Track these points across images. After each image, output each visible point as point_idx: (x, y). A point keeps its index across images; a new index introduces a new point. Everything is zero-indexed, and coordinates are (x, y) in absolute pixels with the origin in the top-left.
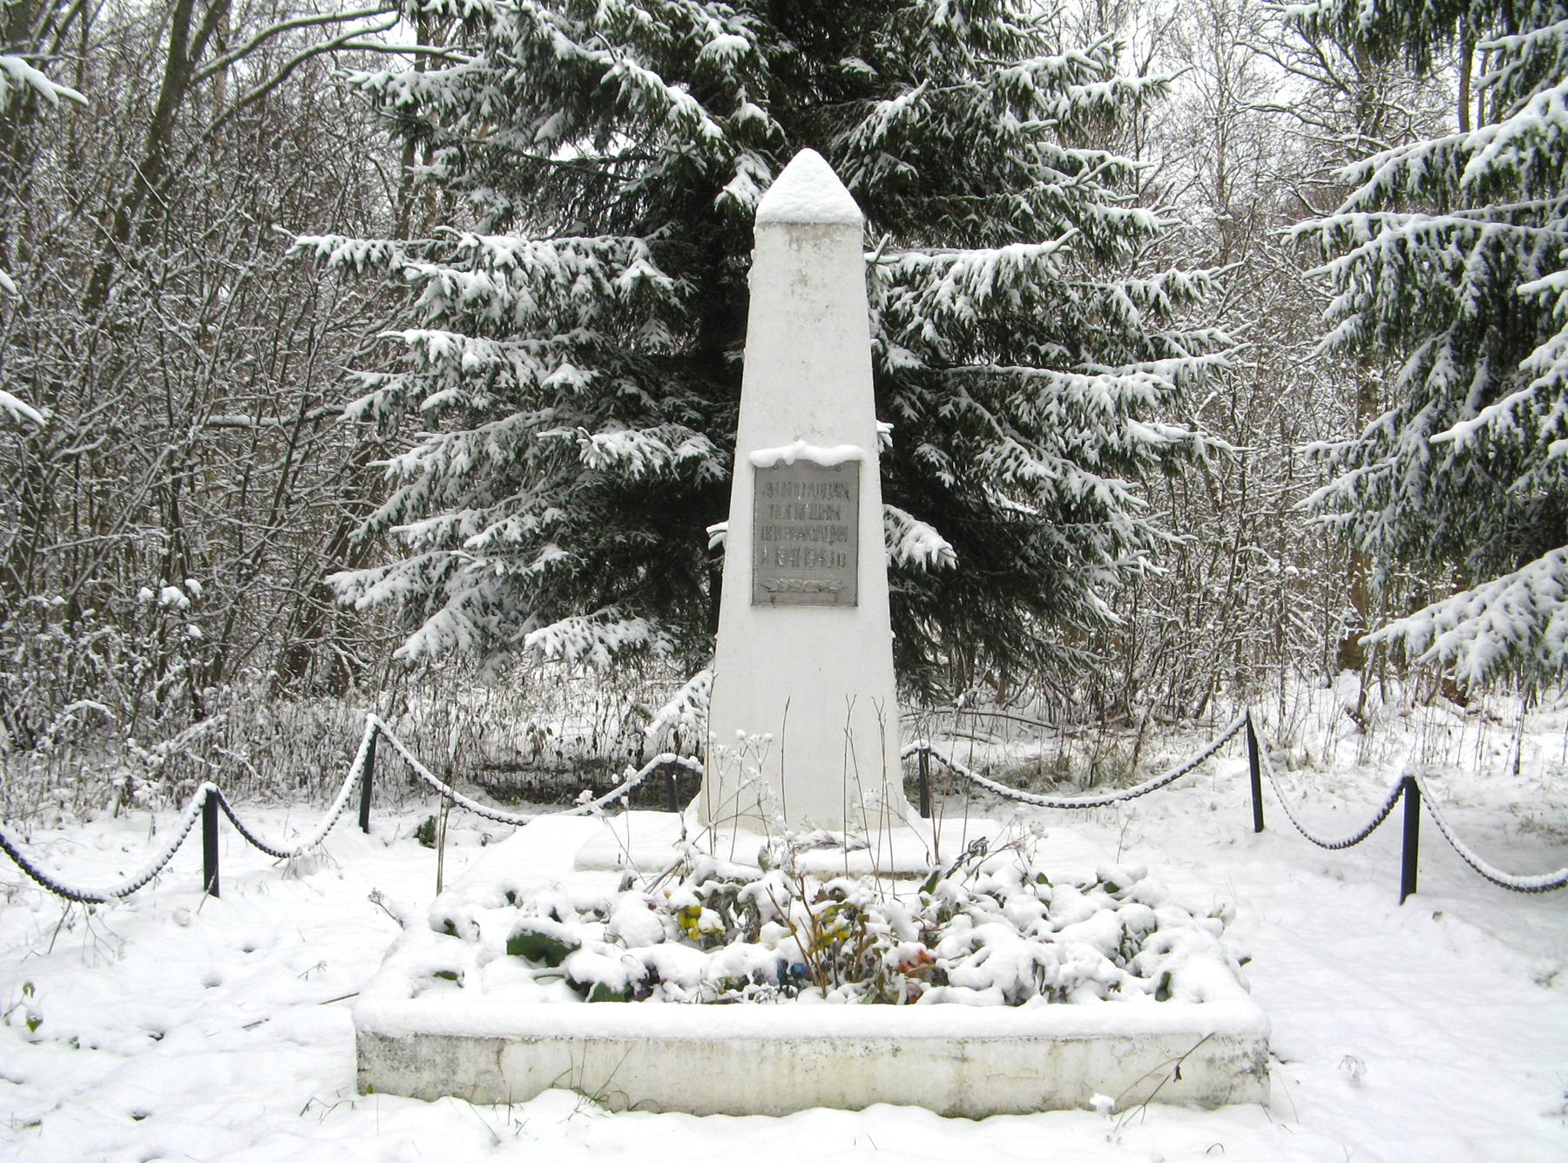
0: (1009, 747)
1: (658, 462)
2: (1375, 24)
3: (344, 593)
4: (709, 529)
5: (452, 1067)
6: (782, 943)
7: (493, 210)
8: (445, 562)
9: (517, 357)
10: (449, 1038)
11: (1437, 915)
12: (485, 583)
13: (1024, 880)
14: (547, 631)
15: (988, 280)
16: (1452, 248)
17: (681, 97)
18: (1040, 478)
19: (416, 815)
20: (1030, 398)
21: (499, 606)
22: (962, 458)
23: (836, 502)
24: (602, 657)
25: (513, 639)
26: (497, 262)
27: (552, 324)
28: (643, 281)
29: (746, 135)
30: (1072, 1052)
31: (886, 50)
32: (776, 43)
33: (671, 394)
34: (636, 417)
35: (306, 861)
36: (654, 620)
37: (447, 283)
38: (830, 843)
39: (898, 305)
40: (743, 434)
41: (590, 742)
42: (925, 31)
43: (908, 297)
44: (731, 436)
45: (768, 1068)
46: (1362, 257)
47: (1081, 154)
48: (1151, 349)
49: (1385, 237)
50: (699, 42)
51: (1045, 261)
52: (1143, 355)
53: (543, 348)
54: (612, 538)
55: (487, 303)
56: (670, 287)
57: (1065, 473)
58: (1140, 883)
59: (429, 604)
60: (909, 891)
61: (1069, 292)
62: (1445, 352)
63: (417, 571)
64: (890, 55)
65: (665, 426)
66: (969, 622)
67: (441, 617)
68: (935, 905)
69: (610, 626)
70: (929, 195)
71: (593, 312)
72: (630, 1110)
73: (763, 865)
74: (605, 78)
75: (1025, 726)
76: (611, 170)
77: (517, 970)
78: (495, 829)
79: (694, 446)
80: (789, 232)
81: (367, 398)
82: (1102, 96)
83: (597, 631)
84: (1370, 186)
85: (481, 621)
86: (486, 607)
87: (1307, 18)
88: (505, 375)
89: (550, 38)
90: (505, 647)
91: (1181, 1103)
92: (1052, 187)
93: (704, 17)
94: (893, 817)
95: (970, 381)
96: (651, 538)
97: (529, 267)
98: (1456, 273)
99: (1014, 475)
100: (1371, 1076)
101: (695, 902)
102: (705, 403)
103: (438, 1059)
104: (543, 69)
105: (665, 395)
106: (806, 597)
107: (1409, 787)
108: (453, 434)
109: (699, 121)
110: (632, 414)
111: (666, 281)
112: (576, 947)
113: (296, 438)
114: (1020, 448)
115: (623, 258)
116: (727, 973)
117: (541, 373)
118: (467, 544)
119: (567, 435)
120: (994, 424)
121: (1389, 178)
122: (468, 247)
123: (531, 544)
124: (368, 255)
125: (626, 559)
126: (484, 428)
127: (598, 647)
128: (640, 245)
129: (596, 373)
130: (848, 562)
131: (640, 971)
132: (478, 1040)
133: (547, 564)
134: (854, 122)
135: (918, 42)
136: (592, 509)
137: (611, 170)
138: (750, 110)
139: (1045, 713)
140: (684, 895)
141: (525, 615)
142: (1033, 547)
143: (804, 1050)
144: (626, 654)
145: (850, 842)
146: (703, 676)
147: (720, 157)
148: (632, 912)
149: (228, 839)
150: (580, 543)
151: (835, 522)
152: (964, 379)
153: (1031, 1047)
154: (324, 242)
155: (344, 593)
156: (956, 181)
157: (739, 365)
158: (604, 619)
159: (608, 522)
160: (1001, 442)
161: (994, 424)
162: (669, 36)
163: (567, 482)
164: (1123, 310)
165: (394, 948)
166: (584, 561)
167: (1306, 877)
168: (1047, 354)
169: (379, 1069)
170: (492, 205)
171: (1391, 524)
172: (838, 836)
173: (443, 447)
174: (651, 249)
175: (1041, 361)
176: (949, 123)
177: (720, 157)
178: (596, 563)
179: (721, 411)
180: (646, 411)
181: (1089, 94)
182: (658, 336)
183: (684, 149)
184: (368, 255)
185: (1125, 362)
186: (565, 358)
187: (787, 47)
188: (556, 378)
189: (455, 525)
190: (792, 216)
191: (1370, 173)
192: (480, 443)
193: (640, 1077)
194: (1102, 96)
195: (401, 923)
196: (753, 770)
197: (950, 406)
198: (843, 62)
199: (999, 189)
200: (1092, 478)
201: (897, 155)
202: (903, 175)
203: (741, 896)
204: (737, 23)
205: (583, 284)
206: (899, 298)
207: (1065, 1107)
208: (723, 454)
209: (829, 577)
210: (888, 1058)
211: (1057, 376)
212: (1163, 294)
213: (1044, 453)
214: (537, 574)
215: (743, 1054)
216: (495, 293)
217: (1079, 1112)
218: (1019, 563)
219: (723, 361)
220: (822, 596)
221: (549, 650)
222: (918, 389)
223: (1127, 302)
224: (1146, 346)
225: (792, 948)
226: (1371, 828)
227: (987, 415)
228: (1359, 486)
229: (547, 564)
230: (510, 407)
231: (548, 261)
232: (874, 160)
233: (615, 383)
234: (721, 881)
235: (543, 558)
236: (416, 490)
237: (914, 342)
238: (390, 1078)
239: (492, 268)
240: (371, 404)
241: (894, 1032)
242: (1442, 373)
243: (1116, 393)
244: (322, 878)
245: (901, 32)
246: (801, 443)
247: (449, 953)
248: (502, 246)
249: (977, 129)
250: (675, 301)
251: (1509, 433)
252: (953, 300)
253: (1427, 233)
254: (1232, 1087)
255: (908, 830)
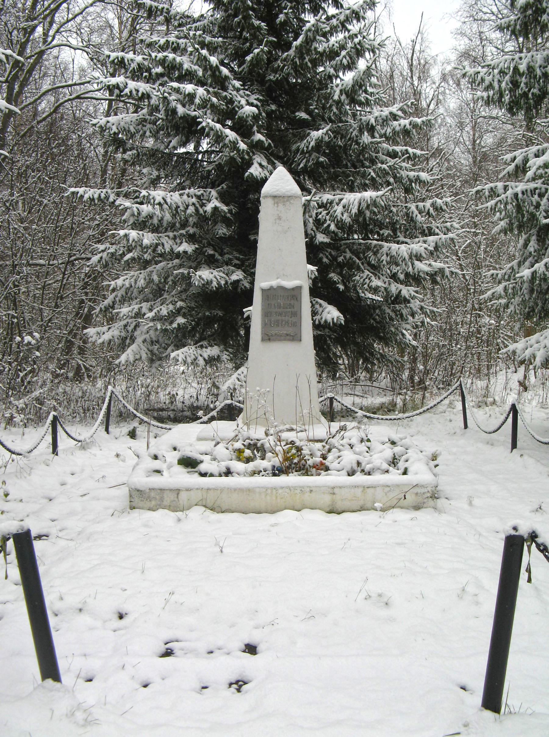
0: (373, 399)
1: (223, 282)
2: (513, 101)
3: (92, 337)
4: (244, 310)
5: (162, 499)
6: (273, 459)
7: (152, 176)
8: (134, 324)
9: (164, 240)
10: (161, 490)
11: (522, 455)
12: (152, 332)
13: (362, 441)
14: (179, 352)
15: (356, 207)
16: (536, 196)
17: (231, 135)
18: (379, 287)
19: (126, 428)
20: (375, 253)
21: (157, 342)
22: (346, 279)
23: (292, 302)
24: (201, 362)
25: (164, 355)
26: (156, 202)
27: (178, 225)
28: (216, 209)
29: (256, 147)
30: (370, 491)
31: (315, 109)
32: (269, 105)
33: (228, 253)
34: (213, 263)
35: (87, 443)
36: (222, 347)
37: (135, 210)
38: (292, 430)
39: (320, 217)
40: (259, 270)
41: (195, 397)
42: (331, 101)
43: (324, 213)
44: (252, 270)
45: (268, 497)
46: (500, 201)
47: (398, 149)
48: (427, 231)
49: (510, 192)
50: (237, 109)
51: (378, 200)
52: (423, 234)
53: (175, 236)
54: (204, 313)
55: (151, 217)
56: (227, 211)
57: (390, 284)
58: (403, 441)
59: (128, 341)
60: (319, 445)
61: (392, 208)
62: (534, 238)
63: (123, 328)
64: (316, 111)
65: (225, 267)
66: (352, 346)
67: (134, 347)
68: (327, 447)
69: (204, 349)
70: (334, 168)
71: (195, 220)
72: (222, 512)
73: (267, 434)
74: (199, 127)
75: (381, 391)
76: (200, 157)
77: (181, 469)
78: (158, 431)
79: (237, 275)
80: (274, 200)
81: (99, 256)
82: (405, 126)
83: (199, 351)
84: (513, 165)
85: (150, 348)
86: (152, 342)
87: (485, 98)
88: (160, 248)
89: (176, 108)
90: (160, 359)
91: (407, 508)
92: (384, 166)
93: (239, 98)
94: (315, 420)
95: (350, 247)
96: (220, 313)
97: (169, 204)
98: (538, 206)
99: (368, 285)
100: (476, 502)
101: (243, 447)
102: (241, 257)
103: (157, 497)
104: (173, 119)
105: (225, 254)
106: (282, 338)
107: (514, 410)
108: (139, 272)
109: (238, 143)
110: (212, 262)
111: (225, 208)
112: (202, 462)
113: (65, 270)
114: (371, 274)
115: (207, 198)
116: (254, 469)
117: (175, 247)
118: (145, 317)
119: (186, 272)
120: (360, 264)
121: (521, 162)
122: (144, 196)
123: (172, 316)
124: (100, 196)
125: (209, 321)
126: (149, 269)
127: (200, 358)
128: (214, 193)
129: (197, 246)
130: (298, 325)
131: (224, 470)
132: (171, 490)
133: (178, 324)
134: (302, 138)
135: (328, 106)
136: (196, 302)
137: (200, 157)
138: (258, 137)
139: (389, 385)
140: (238, 445)
141: (169, 345)
142: (377, 315)
143: (280, 491)
144: (211, 361)
145: (299, 429)
146: (243, 369)
147: (246, 157)
148: (221, 451)
149: (61, 433)
150: (191, 316)
151: (293, 310)
152: (348, 246)
153: (356, 489)
154: (81, 190)
155: (92, 337)
156: (345, 163)
157: (256, 242)
158: (202, 347)
159: (202, 307)
160: (363, 272)
161: (360, 264)
162: (225, 107)
163: (185, 290)
164: (414, 216)
165: (137, 464)
166: (193, 323)
167: (480, 445)
168: (383, 234)
169: (137, 501)
170: (151, 174)
171: (518, 305)
172: (294, 427)
173: (135, 277)
174: (218, 193)
175: (382, 238)
176: (341, 139)
177: (246, 157)
178: (198, 324)
179: (248, 260)
180: (217, 261)
181: (400, 125)
182: (222, 230)
183: (232, 154)
184: (100, 196)
185: (416, 237)
186: (184, 240)
187: (273, 107)
188: (181, 249)
189: (140, 309)
190: (275, 194)
191: (515, 158)
192: (150, 275)
193: (226, 500)
194: (405, 126)
195: (138, 456)
196: (263, 402)
197: (342, 257)
198: (297, 114)
199: (363, 166)
200: (401, 287)
201: (318, 153)
202: (322, 162)
203: (259, 445)
204: (252, 99)
205: (191, 210)
206: (321, 213)
207: (368, 510)
208: (249, 278)
209: (290, 330)
210: (309, 494)
211: (386, 244)
212: (431, 209)
213: (381, 276)
214: (175, 328)
215: (260, 493)
216: (155, 214)
217: (373, 511)
218: (372, 321)
219: (249, 240)
220: (288, 337)
221: (180, 359)
222: (329, 250)
223: (416, 212)
224: (424, 230)
225: (276, 461)
226: (502, 425)
227: (357, 261)
228: (505, 289)
229: (178, 324)
230: (160, 259)
231: (177, 200)
232: (310, 156)
233: (205, 249)
234: (252, 440)
235: (177, 322)
236: (120, 293)
237: (326, 231)
238: (141, 504)
239: (154, 204)
240: (101, 258)
241: (311, 485)
242: (533, 246)
243: (409, 252)
244: (94, 450)
245: (321, 101)
246: (279, 280)
247: (157, 465)
248: (158, 194)
249: (352, 142)
250: (228, 215)
251: (544, 274)
252: (342, 214)
253: (526, 191)
254: (424, 503)
255: (321, 425)
